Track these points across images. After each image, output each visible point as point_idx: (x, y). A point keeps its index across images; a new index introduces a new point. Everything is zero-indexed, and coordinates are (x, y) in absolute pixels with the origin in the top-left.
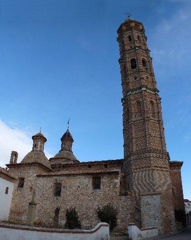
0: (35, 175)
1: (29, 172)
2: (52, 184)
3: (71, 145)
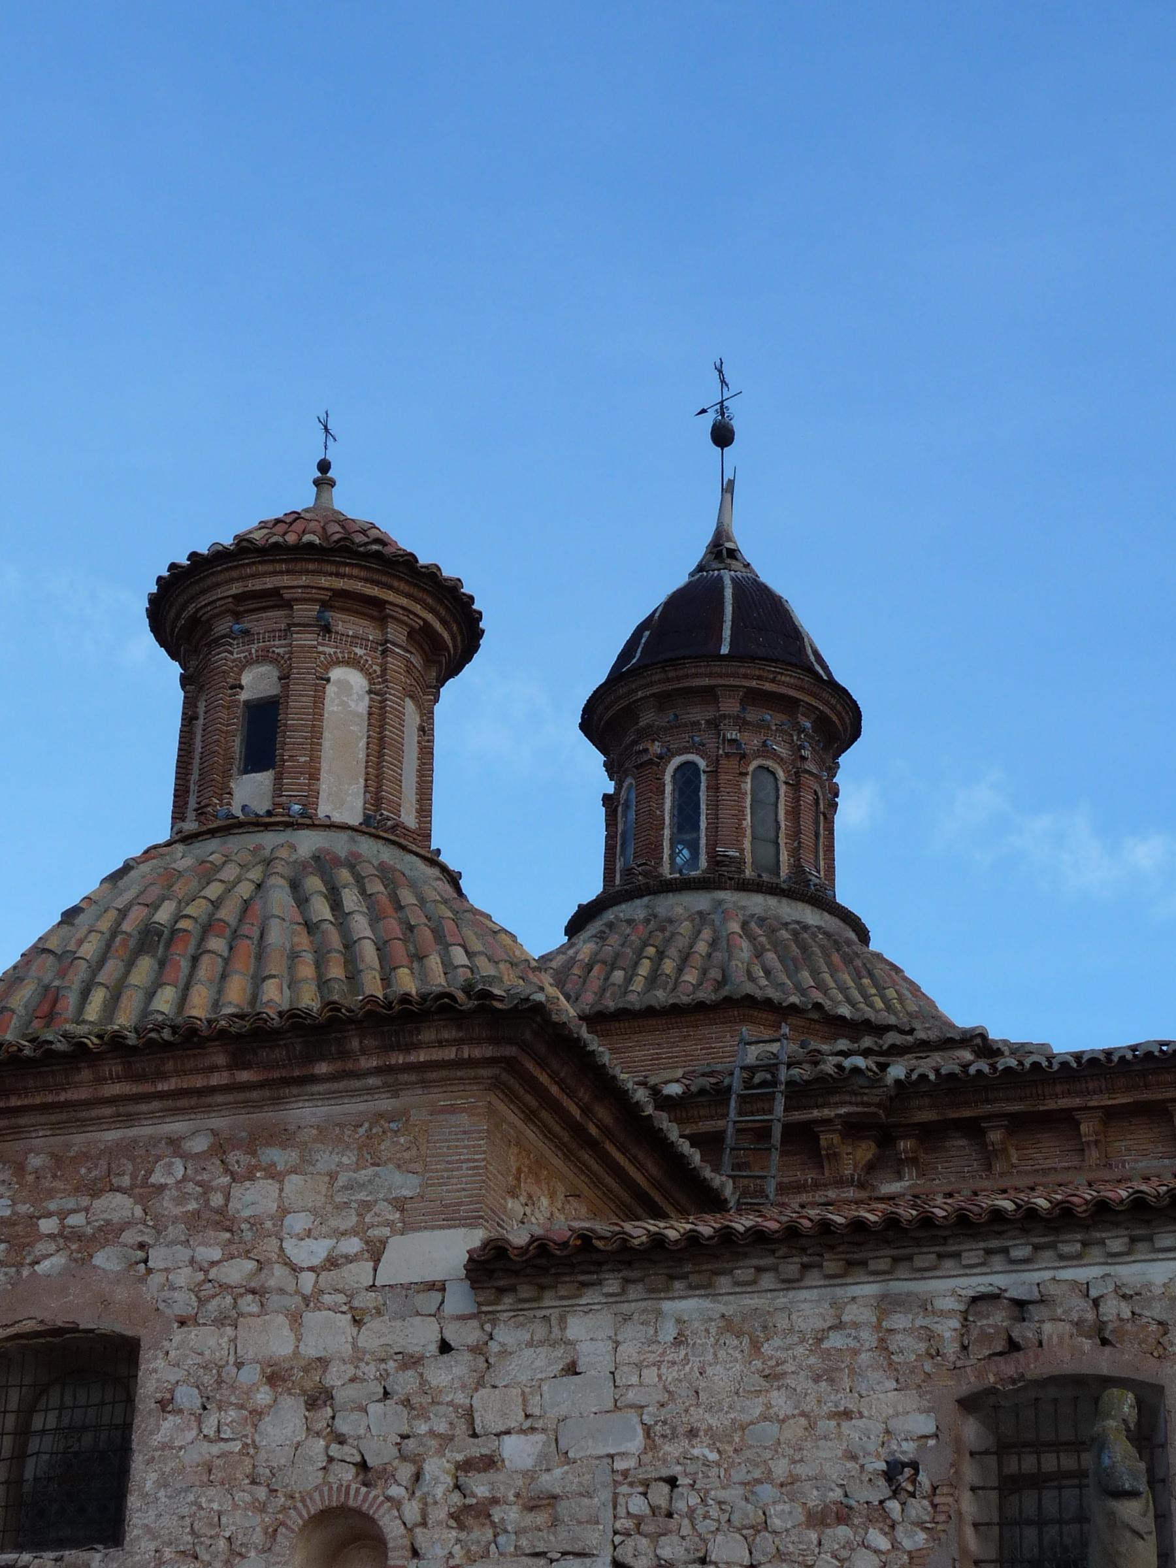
0: (446, 1251)
1: (255, 1199)
2: (903, 1417)
3: (827, 805)
